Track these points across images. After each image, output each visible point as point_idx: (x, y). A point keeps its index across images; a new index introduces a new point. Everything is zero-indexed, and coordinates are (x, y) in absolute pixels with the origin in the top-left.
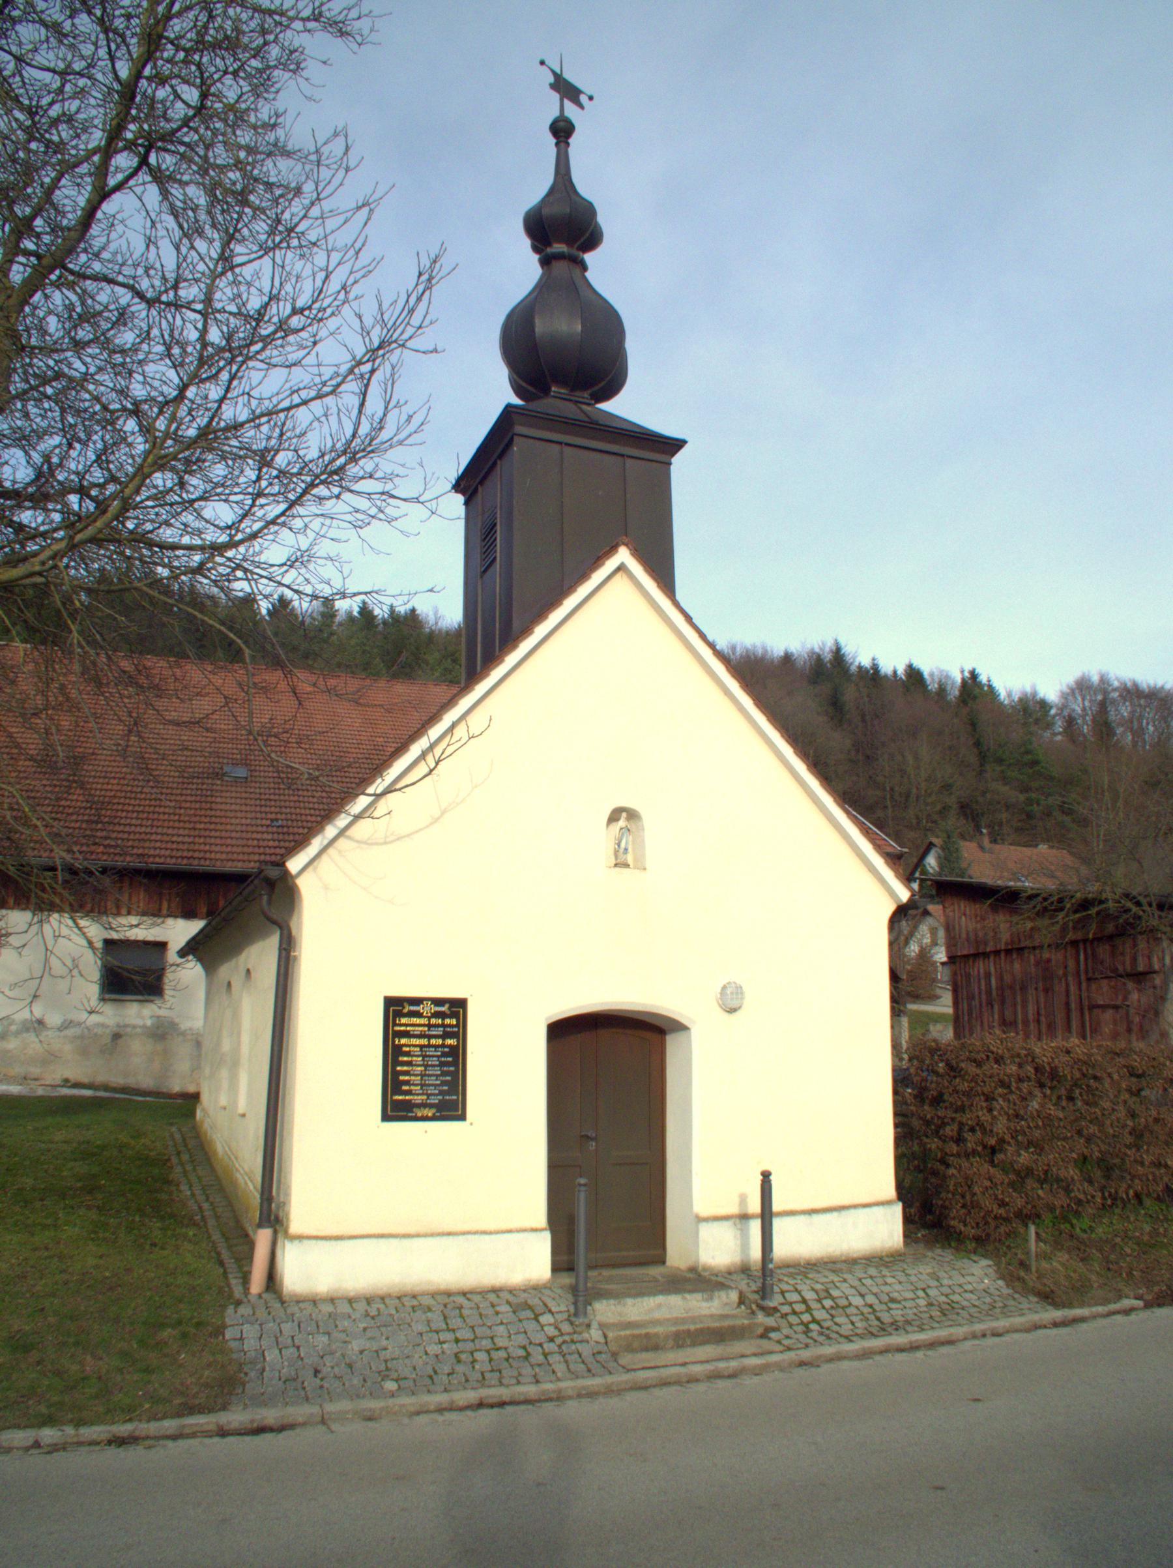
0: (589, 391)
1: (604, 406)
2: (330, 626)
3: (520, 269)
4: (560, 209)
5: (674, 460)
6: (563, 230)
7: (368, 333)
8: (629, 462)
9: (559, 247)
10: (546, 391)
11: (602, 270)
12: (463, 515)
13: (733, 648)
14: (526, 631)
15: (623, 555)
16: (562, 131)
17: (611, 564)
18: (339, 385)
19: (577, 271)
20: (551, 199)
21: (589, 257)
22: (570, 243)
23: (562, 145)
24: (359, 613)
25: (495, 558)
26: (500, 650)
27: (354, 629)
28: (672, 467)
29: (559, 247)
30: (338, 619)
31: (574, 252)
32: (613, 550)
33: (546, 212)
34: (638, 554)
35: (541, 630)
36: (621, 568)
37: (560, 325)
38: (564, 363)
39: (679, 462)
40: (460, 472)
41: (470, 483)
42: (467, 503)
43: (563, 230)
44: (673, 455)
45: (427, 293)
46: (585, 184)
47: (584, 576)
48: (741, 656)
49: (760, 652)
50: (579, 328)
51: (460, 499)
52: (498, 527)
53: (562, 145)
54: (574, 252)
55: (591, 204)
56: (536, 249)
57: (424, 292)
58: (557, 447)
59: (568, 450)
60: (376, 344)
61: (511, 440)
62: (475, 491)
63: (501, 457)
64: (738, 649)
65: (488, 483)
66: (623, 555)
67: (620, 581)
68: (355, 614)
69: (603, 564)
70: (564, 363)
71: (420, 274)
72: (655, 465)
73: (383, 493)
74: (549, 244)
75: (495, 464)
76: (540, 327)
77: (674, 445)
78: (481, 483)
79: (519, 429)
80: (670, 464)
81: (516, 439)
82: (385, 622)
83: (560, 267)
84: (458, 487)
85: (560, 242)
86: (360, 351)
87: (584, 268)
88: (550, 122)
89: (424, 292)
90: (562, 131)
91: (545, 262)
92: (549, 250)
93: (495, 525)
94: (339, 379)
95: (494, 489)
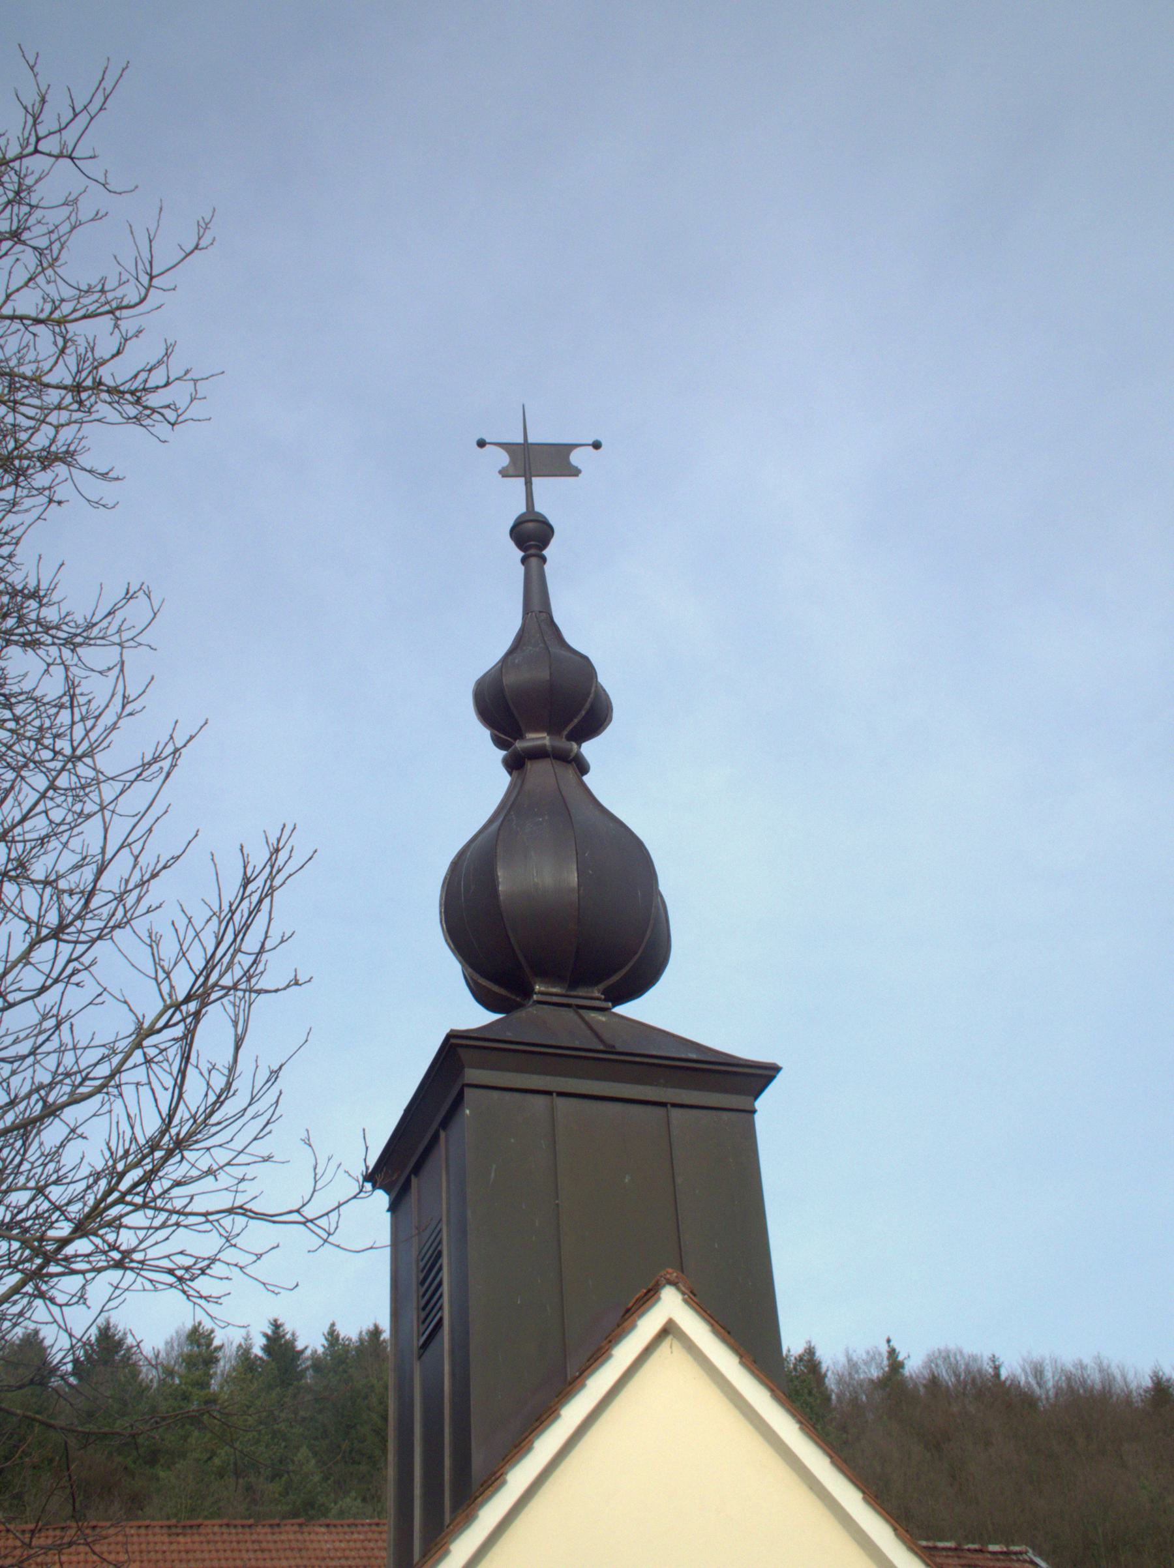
0: (602, 986)
1: (627, 1010)
2: (204, 1385)
3: (473, 782)
4: (534, 674)
5: (759, 1104)
6: (543, 707)
7: (168, 975)
8: (675, 1113)
9: (537, 739)
10: (527, 992)
11: (617, 773)
12: (385, 1237)
13: (1038, 1372)
14: (493, 1481)
15: (671, 1305)
16: (532, 536)
17: (648, 1325)
18: (117, 1071)
19: (570, 773)
20: (518, 658)
21: (589, 749)
22: (554, 728)
23: (534, 561)
24: (266, 1349)
25: (440, 1322)
26: (455, 1508)
27: (255, 1386)
28: (757, 1117)
29: (537, 739)
30: (224, 1366)
31: (562, 743)
32: (649, 1296)
33: (509, 680)
34: (698, 1301)
35: (520, 1477)
36: (669, 1330)
37: (541, 875)
38: (554, 934)
39: (768, 1107)
40: (372, 1162)
41: (400, 1168)
42: (393, 1208)
43: (543, 707)
44: (757, 1096)
45: (267, 901)
46: (581, 625)
47: (598, 1356)
48: (1057, 1387)
49: (1095, 1378)
50: (573, 879)
51: (381, 1199)
52: (445, 1260)
53: (534, 561)
54: (562, 743)
55: (586, 659)
56: (500, 743)
57: (260, 901)
58: (541, 1100)
59: (560, 1102)
60: (181, 998)
61: (459, 1100)
62: (406, 1187)
63: (445, 1124)
64: (1048, 1375)
65: (429, 1165)
66: (671, 1305)
67: (669, 1354)
68: (257, 1351)
69: (633, 1326)
70: (554, 934)
71: (247, 882)
72: (725, 1116)
73: (230, 1211)
74: (519, 735)
75: (435, 1138)
76: (507, 881)
77: (760, 1076)
78: (417, 1169)
79: (473, 1075)
80: (754, 1112)
81: (468, 1092)
82: (318, 1364)
83: (539, 770)
84: (376, 1177)
85: (536, 730)
86: (150, 1007)
87: (582, 767)
88: (511, 523)
89: (260, 901)
90: (532, 536)
91: (514, 764)
92: (519, 745)
93: (440, 1254)
94: (116, 1060)
95: (435, 1186)
